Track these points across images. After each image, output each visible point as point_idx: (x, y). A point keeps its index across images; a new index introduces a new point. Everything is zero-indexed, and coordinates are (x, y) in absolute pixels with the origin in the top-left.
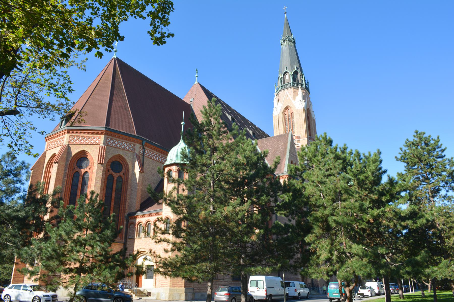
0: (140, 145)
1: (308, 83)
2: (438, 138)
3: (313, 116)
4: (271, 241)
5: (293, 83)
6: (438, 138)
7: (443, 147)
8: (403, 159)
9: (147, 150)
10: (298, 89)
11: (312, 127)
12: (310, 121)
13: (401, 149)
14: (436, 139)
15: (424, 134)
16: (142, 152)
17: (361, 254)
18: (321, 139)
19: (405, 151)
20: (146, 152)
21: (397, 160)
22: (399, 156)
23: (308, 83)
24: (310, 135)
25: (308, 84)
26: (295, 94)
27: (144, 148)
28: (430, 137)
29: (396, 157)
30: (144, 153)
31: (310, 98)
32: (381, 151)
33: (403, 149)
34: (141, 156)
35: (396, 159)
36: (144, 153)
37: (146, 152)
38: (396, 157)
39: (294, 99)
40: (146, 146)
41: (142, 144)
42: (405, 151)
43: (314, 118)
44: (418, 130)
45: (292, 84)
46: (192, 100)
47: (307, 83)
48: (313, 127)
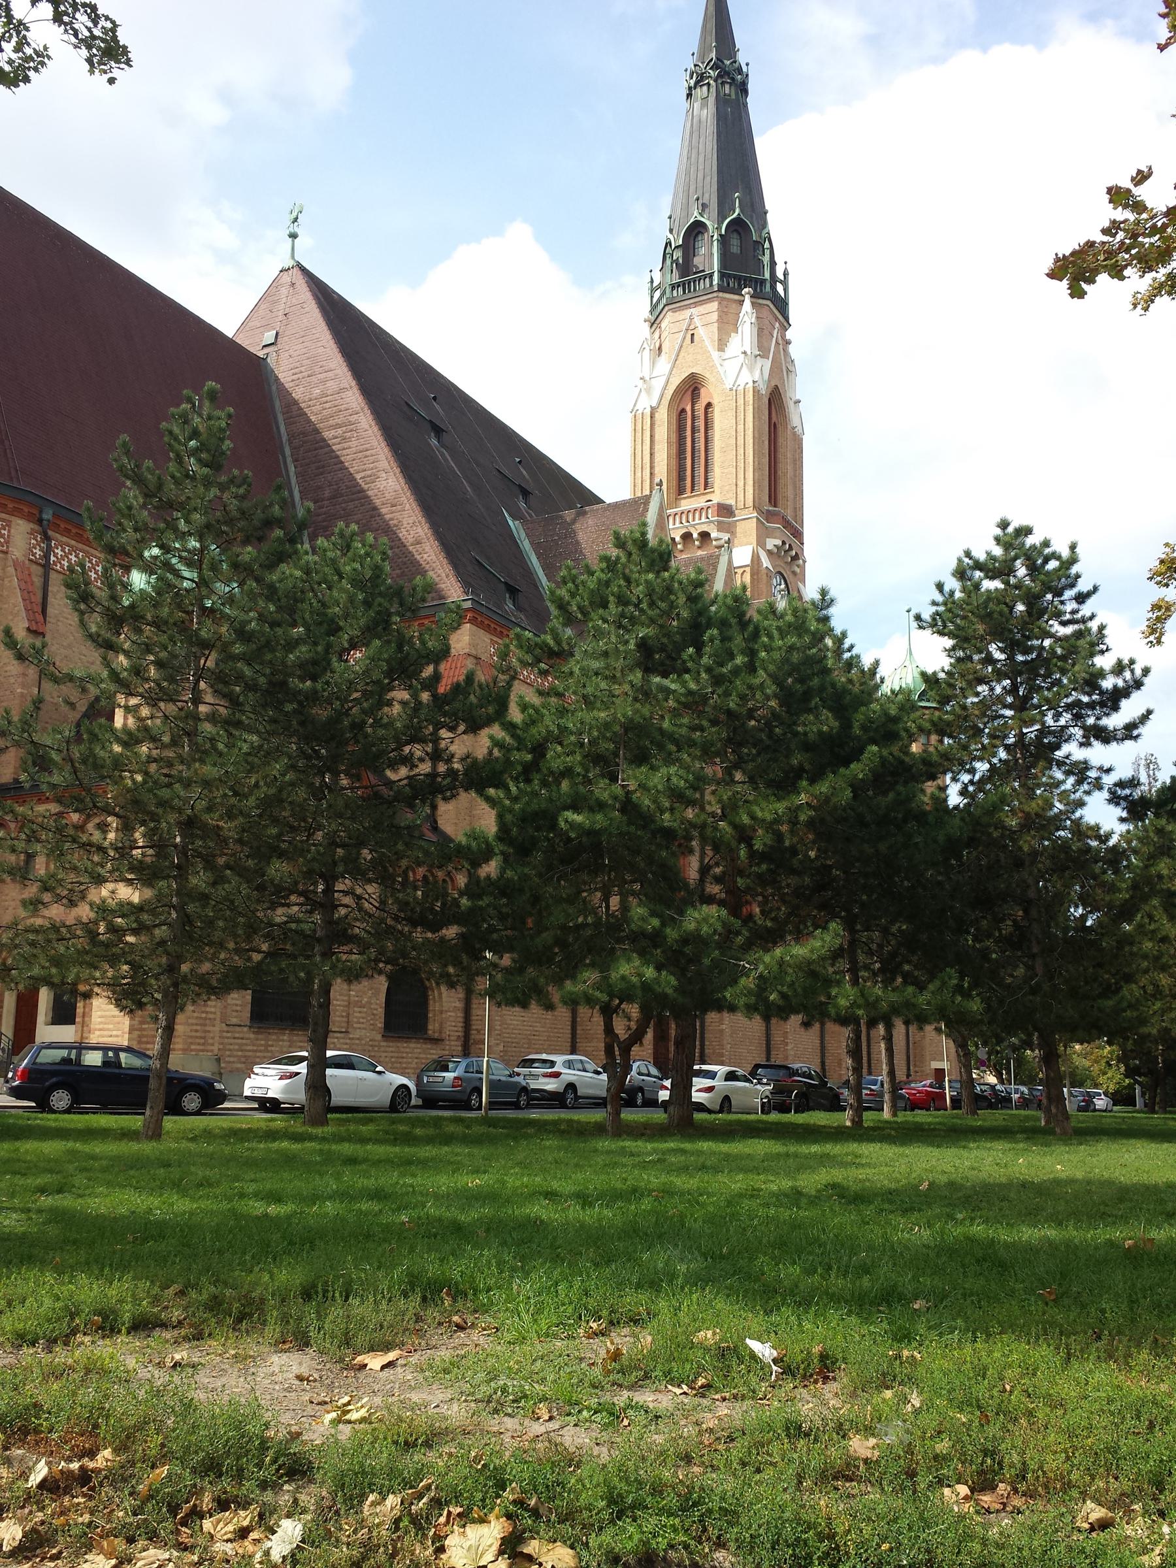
0: (32, 525)
1: (786, 274)
2: (1073, 547)
3: (795, 421)
4: (994, 956)
5: (722, 276)
6: (1073, 547)
7: (1083, 586)
8: (938, 624)
9: (62, 545)
10: (741, 302)
11: (785, 467)
12: (781, 440)
13: (940, 587)
14: (1065, 553)
15: (1028, 531)
16: (38, 552)
17: (40, 906)
18: (630, 546)
19: (952, 593)
20: (59, 552)
21: (920, 627)
22: (926, 616)
23: (786, 274)
24: (773, 499)
25: (785, 283)
26: (727, 324)
27: (47, 538)
28: (1046, 544)
29: (918, 618)
30: (46, 556)
31: (788, 342)
32: (833, 593)
33: (947, 589)
34: (34, 568)
35: (914, 624)
36: (46, 556)
37: (59, 552)
38: (918, 618)
39: (722, 345)
40: (56, 528)
41: (40, 521)
42: (952, 593)
43: (798, 430)
44: (1010, 518)
45: (715, 282)
46: (269, 337)
47: (780, 274)
48: (790, 473)
